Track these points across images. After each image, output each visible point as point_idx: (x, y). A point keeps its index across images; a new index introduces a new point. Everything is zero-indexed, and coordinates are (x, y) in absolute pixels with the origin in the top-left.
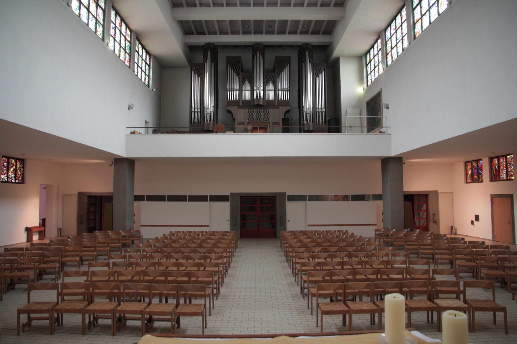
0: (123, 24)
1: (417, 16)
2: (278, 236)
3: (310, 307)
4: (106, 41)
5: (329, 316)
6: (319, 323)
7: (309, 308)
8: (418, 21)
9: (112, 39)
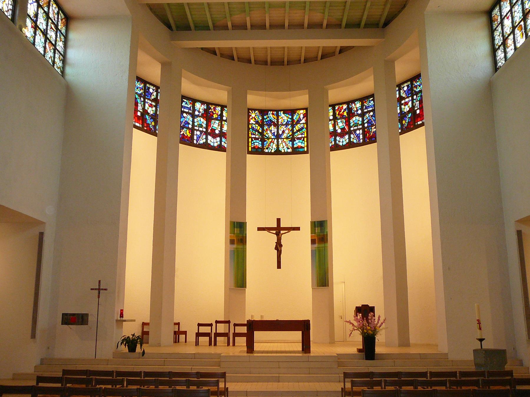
9: (29, 22)
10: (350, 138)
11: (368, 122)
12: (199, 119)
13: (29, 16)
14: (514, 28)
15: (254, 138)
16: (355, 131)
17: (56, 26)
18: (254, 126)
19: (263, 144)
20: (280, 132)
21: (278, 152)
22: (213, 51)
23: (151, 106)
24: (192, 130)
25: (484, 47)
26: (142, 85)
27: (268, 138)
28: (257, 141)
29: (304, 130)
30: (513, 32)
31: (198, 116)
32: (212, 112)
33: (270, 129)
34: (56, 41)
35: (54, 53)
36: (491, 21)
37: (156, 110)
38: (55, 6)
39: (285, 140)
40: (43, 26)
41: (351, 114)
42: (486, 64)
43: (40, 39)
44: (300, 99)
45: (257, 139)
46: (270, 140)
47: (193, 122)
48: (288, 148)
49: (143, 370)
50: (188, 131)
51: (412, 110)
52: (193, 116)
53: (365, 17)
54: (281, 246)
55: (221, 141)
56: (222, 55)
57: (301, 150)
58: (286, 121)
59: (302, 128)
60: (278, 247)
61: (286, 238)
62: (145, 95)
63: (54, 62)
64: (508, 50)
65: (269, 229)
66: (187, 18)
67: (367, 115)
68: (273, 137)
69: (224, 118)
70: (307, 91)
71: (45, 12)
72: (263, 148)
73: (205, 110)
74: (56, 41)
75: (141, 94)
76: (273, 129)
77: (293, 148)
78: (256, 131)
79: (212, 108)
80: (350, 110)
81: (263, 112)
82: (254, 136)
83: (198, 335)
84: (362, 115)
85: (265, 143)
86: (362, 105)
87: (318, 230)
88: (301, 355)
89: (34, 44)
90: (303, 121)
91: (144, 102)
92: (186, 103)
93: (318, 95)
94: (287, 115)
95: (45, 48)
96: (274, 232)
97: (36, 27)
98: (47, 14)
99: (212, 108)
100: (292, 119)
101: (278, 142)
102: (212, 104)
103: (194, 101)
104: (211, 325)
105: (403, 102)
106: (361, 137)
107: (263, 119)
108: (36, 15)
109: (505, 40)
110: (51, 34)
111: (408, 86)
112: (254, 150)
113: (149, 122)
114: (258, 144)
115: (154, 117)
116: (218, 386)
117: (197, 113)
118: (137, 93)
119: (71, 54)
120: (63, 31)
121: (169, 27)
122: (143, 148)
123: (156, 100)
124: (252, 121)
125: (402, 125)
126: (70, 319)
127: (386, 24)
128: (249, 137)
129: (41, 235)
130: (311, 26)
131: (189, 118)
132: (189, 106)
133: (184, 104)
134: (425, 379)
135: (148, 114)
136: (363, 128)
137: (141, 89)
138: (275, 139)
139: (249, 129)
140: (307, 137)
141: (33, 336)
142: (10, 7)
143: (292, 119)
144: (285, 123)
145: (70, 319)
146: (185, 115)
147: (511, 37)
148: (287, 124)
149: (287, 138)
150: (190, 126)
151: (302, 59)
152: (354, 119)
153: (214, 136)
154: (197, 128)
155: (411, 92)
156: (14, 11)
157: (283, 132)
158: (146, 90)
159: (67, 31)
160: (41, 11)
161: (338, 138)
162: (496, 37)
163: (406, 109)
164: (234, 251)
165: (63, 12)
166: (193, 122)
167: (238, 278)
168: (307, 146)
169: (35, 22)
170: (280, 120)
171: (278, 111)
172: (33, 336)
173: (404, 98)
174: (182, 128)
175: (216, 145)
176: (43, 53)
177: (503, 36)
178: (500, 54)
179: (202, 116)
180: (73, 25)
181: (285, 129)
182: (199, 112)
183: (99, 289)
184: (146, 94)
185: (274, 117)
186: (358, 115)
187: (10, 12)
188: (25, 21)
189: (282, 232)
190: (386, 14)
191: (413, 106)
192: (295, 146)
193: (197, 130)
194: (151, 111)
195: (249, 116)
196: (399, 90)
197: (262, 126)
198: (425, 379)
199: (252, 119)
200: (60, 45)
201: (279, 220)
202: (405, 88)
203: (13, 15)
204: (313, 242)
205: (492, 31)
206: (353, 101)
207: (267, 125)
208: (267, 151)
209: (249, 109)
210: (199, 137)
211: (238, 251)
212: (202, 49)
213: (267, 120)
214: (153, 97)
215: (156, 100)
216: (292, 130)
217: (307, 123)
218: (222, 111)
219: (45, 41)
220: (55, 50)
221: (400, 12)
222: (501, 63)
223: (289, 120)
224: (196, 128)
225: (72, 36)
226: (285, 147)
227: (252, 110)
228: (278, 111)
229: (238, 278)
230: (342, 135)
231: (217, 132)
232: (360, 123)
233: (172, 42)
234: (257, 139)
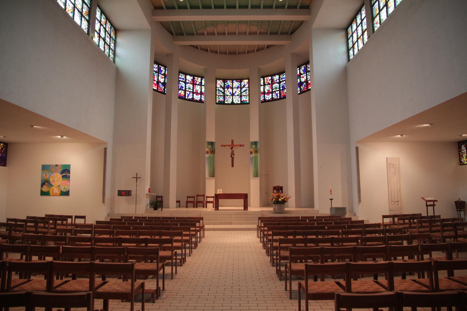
0: (108, 22)
1: (376, 11)
2: (68, 190)
3: (288, 289)
4: (91, 35)
5: (315, 301)
6: (288, 287)
7: (286, 290)
8: (376, 16)
9: (96, 35)
10: (272, 95)
11: (282, 87)
12: (189, 84)
13: (96, 31)
14: (358, 39)
16: (275, 91)
17: (110, 35)
19: (224, 99)
20: (234, 92)
22: (196, 47)
23: (162, 78)
24: (185, 91)
25: (344, 49)
27: (227, 96)
29: (247, 91)
30: (357, 41)
31: (188, 83)
34: (110, 43)
35: (109, 50)
36: (347, 34)
37: (165, 80)
38: (109, 24)
40: (103, 36)
41: (273, 82)
42: (345, 58)
43: (102, 42)
47: (186, 86)
51: (306, 81)
52: (185, 83)
53: (280, 29)
54: (234, 155)
55: (201, 97)
56: (201, 49)
57: (246, 102)
59: (246, 90)
62: (159, 72)
63: (109, 55)
64: (355, 50)
66: (182, 29)
67: (282, 83)
69: (203, 84)
71: (104, 28)
72: (224, 101)
74: (110, 43)
76: (230, 90)
77: (241, 101)
78: (221, 91)
80: (272, 80)
83: (188, 202)
84: (279, 83)
86: (279, 77)
87: (254, 146)
89: (99, 46)
90: (247, 86)
91: (158, 76)
95: (104, 47)
97: (100, 37)
98: (105, 29)
100: (241, 85)
101: (233, 98)
102: (196, 76)
104: (194, 197)
105: (301, 76)
106: (279, 95)
108: (100, 30)
109: (354, 45)
110: (108, 40)
111: (304, 67)
113: (161, 86)
114: (221, 99)
115: (164, 84)
118: (154, 71)
119: (118, 50)
120: (114, 37)
121: (172, 34)
123: (164, 74)
125: (301, 89)
126: (121, 193)
127: (292, 33)
129: (106, 149)
131: (183, 84)
133: (180, 76)
135: (160, 82)
136: (280, 90)
139: (216, 90)
140: (249, 95)
141: (104, 202)
142: (87, 27)
143: (241, 85)
146: (181, 82)
147: (357, 43)
148: (238, 88)
149: (238, 95)
150: (184, 89)
151: (246, 52)
152: (275, 85)
153: (197, 94)
155: (306, 71)
156: (88, 29)
158: (159, 69)
159: (116, 37)
160: (102, 27)
161: (266, 96)
162: (350, 43)
163: (303, 80)
165: (113, 27)
166: (186, 86)
168: (249, 100)
169: (99, 34)
172: (104, 202)
173: (302, 74)
174: (180, 90)
175: (198, 99)
176: (103, 50)
177: (353, 42)
178: (351, 52)
180: (119, 35)
183: (137, 178)
184: (159, 71)
186: (277, 83)
187: (87, 29)
188: (94, 35)
190: (291, 28)
191: (307, 79)
192: (242, 100)
194: (162, 80)
195: (216, 83)
196: (300, 69)
197: (224, 88)
200: (112, 45)
201: (232, 141)
202: (303, 68)
203: (88, 31)
205: (348, 39)
206: (275, 75)
210: (188, 95)
211: (210, 158)
214: (163, 73)
215: (164, 74)
216: (241, 91)
217: (249, 87)
218: (201, 80)
219: (105, 44)
220: (110, 48)
221: (300, 26)
222: (351, 57)
225: (118, 40)
230: (268, 93)
231: (199, 92)
232: (278, 87)
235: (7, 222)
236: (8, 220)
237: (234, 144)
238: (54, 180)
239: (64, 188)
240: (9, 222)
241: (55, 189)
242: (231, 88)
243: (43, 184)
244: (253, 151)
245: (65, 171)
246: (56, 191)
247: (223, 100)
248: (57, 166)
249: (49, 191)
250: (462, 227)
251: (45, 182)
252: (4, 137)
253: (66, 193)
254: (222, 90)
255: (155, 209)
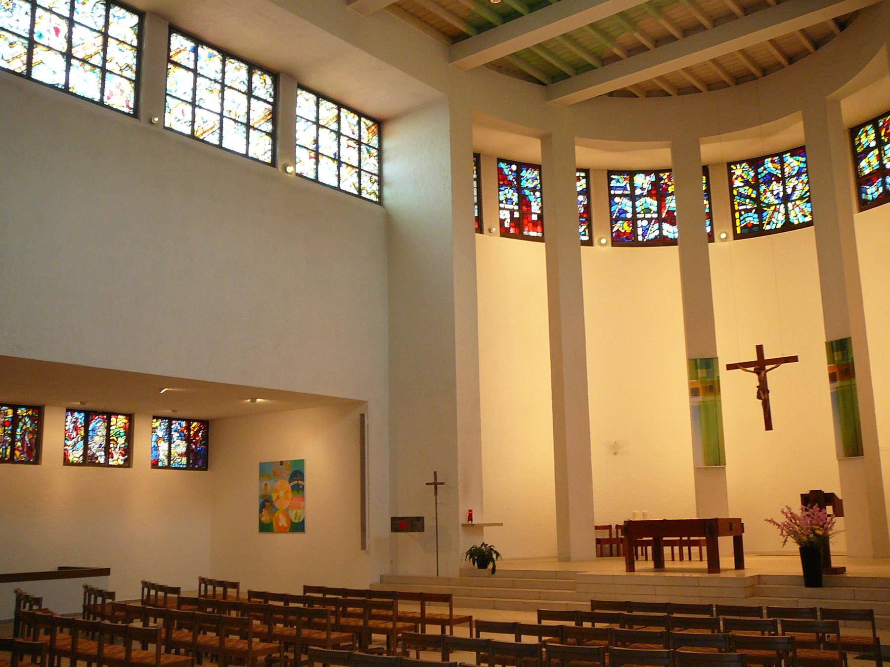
12: (643, 200)
15: (743, 210)
18: (741, 190)
19: (761, 218)
20: (789, 191)
21: (788, 226)
24: (633, 221)
26: (536, 173)
27: (769, 206)
28: (750, 214)
31: (641, 196)
32: (666, 184)
33: (771, 188)
35: (359, 176)
39: (798, 202)
44: (794, 131)
45: (750, 211)
46: (773, 208)
47: (634, 207)
48: (805, 216)
49: (714, 602)
50: (626, 224)
52: (633, 198)
58: (797, 169)
60: (763, 392)
61: (773, 376)
65: (744, 365)
68: (777, 202)
70: (799, 113)
72: (761, 225)
73: (652, 183)
75: (535, 187)
76: (776, 187)
79: (665, 177)
81: (756, 163)
82: (744, 207)
85: (765, 214)
87: (702, 373)
88: (652, 574)
92: (618, 181)
93: (819, 116)
94: (798, 158)
96: (752, 369)
99: (665, 177)
101: (786, 208)
102: (664, 171)
103: (631, 174)
107: (757, 174)
112: (745, 231)
116: (837, 632)
117: (638, 192)
120: (375, 142)
122: (514, 271)
124: (737, 183)
126: (401, 525)
128: (733, 212)
130: (687, 31)
131: (627, 204)
132: (623, 185)
133: (613, 183)
134: (708, 616)
137: (534, 179)
138: (780, 204)
139: (732, 197)
141: (364, 547)
144: (795, 172)
145: (401, 525)
146: (617, 200)
148: (799, 174)
150: (629, 216)
154: (641, 216)
157: (794, 188)
164: (699, 406)
166: (634, 207)
167: (711, 454)
170: (787, 170)
171: (781, 155)
172: (364, 547)
174: (614, 221)
179: (650, 194)
180: (388, 130)
181: (796, 182)
182: (642, 189)
183: (436, 484)
185: (776, 165)
189: (767, 367)
193: (642, 219)
195: (730, 174)
197: (755, 187)
198: (708, 616)
199: (736, 179)
200: (370, 164)
201: (760, 349)
204: (694, 392)
207: (764, 183)
208: (768, 228)
209: (729, 164)
212: (611, 94)
213: (763, 175)
223: (802, 165)
224: (638, 216)
226: (800, 215)
227: (735, 163)
228: (781, 155)
229: (711, 454)
233: (549, 103)
234: (750, 211)
235: (305, 593)
236: (307, 589)
237: (767, 357)
238: (278, 497)
239: (296, 514)
240: (307, 594)
241: (281, 516)
242: (778, 180)
243: (262, 507)
244: (699, 386)
245: (297, 474)
246: (283, 522)
247: (756, 222)
248: (282, 463)
249: (272, 523)
250: (545, 623)
251: (266, 503)
252: (173, 411)
253: (298, 527)
254: (748, 191)
255: (480, 567)
